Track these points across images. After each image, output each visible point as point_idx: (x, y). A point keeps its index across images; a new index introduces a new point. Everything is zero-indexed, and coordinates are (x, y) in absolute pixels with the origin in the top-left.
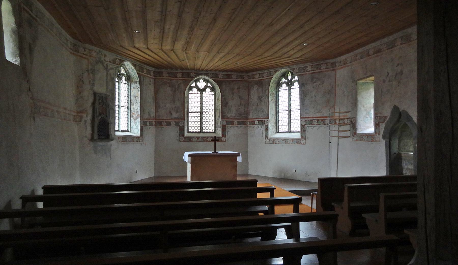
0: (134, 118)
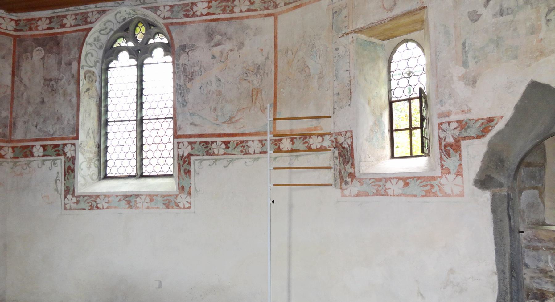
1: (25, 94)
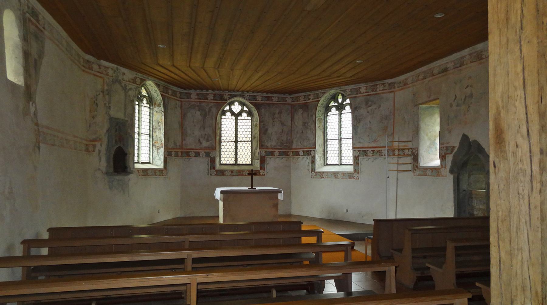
0: (157, 147)
1: (296, 129)
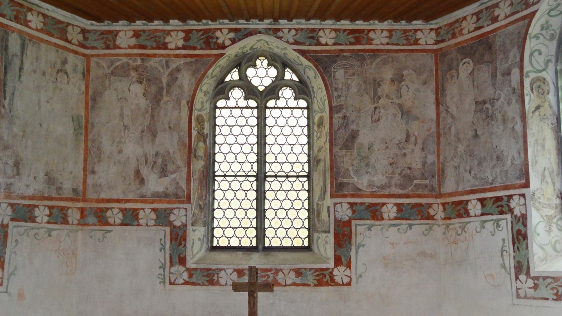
1: (453, 128)
